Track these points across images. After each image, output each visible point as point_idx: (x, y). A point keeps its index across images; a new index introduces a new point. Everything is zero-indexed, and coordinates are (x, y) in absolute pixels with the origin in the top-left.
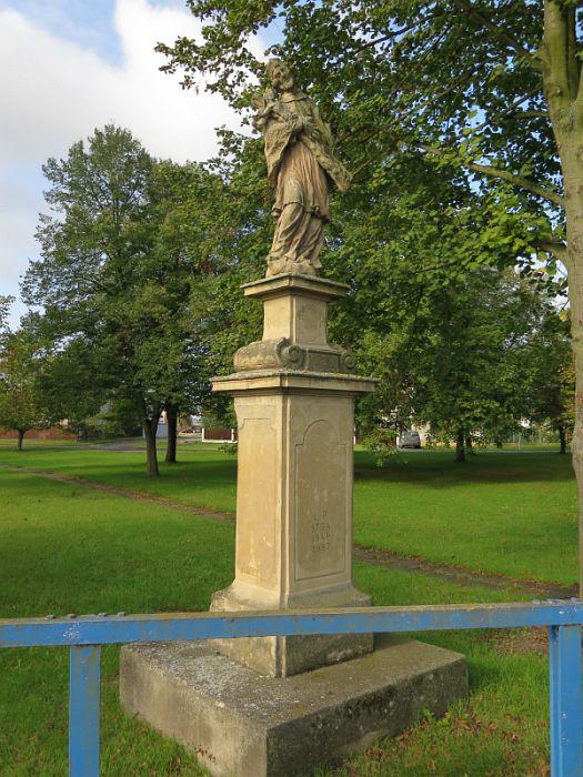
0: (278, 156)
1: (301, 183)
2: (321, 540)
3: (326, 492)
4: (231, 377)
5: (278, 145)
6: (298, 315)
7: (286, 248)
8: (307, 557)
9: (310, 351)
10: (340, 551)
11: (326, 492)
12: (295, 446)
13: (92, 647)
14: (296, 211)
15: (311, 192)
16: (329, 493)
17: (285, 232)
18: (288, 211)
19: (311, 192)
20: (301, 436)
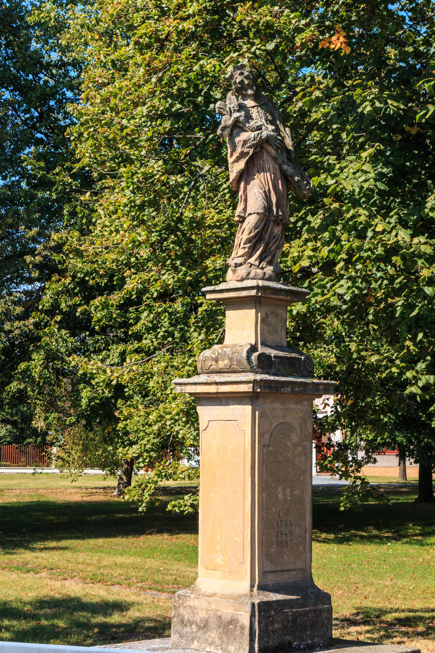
0: (241, 164)
1: (265, 192)
2: (284, 536)
3: (288, 491)
4: (190, 380)
5: (242, 155)
6: (263, 321)
7: (249, 255)
8: (272, 550)
9: (275, 357)
10: (301, 549)
11: (288, 491)
12: (262, 446)
13: (163, 651)
14: (260, 221)
15: (274, 199)
16: (291, 492)
17: (249, 241)
18: (251, 221)
19: (274, 199)
20: (267, 436)
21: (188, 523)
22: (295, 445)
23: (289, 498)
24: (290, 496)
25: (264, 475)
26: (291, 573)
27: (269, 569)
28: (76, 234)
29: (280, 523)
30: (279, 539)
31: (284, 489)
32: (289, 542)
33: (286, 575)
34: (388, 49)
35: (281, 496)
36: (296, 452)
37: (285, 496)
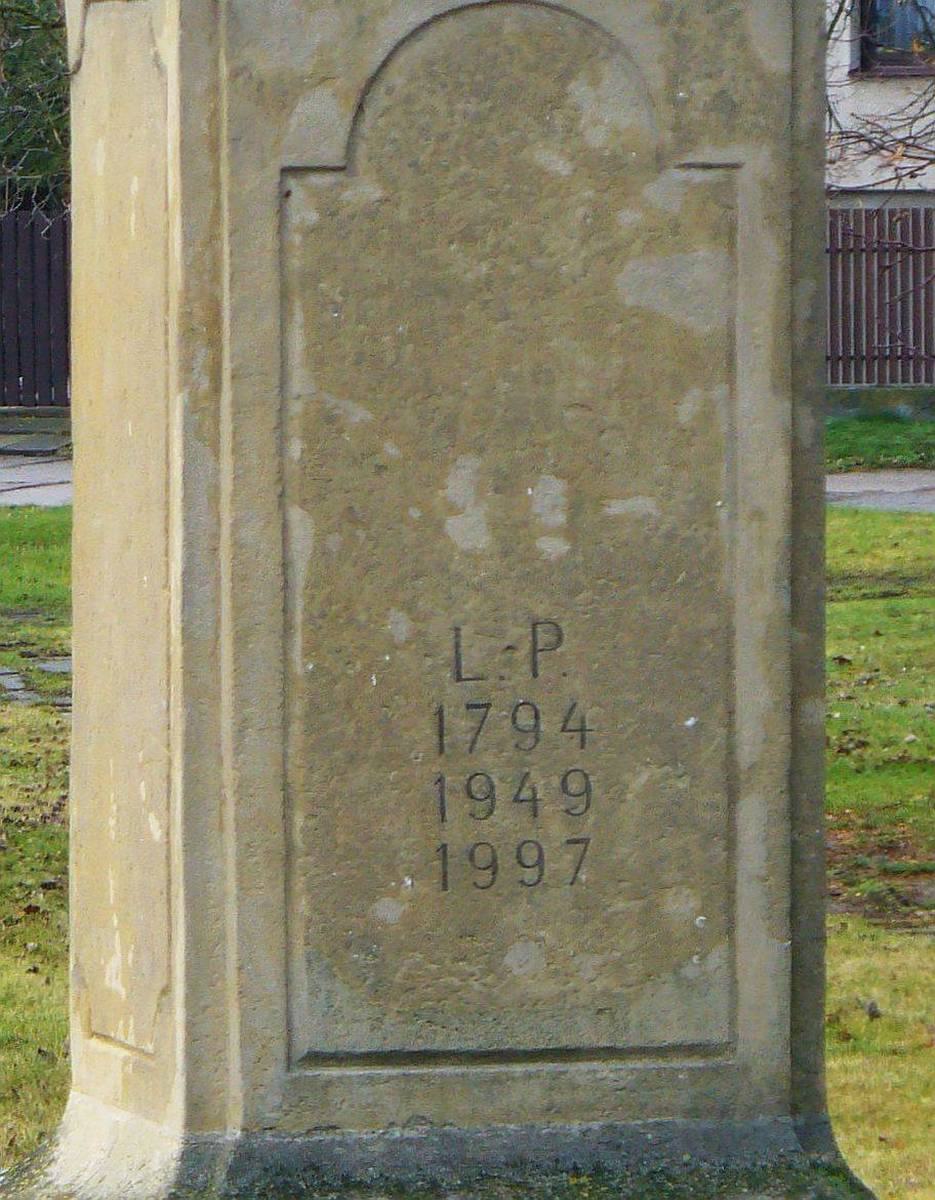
8: (388, 910)
10: (682, 906)
11: (547, 497)
21: (71, 655)
22: (613, 171)
23: (553, 547)
24: (570, 532)
25: (300, 381)
26: (578, 1069)
27: (363, 1039)
28: (452, 567)
29: (460, 725)
30: (458, 832)
31: (505, 484)
32: (560, 863)
33: (525, 1090)
34: (406, 879)
35: (469, 531)
36: (628, 217)
37: (513, 534)
